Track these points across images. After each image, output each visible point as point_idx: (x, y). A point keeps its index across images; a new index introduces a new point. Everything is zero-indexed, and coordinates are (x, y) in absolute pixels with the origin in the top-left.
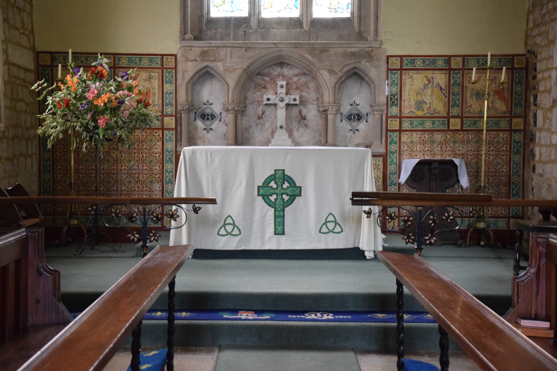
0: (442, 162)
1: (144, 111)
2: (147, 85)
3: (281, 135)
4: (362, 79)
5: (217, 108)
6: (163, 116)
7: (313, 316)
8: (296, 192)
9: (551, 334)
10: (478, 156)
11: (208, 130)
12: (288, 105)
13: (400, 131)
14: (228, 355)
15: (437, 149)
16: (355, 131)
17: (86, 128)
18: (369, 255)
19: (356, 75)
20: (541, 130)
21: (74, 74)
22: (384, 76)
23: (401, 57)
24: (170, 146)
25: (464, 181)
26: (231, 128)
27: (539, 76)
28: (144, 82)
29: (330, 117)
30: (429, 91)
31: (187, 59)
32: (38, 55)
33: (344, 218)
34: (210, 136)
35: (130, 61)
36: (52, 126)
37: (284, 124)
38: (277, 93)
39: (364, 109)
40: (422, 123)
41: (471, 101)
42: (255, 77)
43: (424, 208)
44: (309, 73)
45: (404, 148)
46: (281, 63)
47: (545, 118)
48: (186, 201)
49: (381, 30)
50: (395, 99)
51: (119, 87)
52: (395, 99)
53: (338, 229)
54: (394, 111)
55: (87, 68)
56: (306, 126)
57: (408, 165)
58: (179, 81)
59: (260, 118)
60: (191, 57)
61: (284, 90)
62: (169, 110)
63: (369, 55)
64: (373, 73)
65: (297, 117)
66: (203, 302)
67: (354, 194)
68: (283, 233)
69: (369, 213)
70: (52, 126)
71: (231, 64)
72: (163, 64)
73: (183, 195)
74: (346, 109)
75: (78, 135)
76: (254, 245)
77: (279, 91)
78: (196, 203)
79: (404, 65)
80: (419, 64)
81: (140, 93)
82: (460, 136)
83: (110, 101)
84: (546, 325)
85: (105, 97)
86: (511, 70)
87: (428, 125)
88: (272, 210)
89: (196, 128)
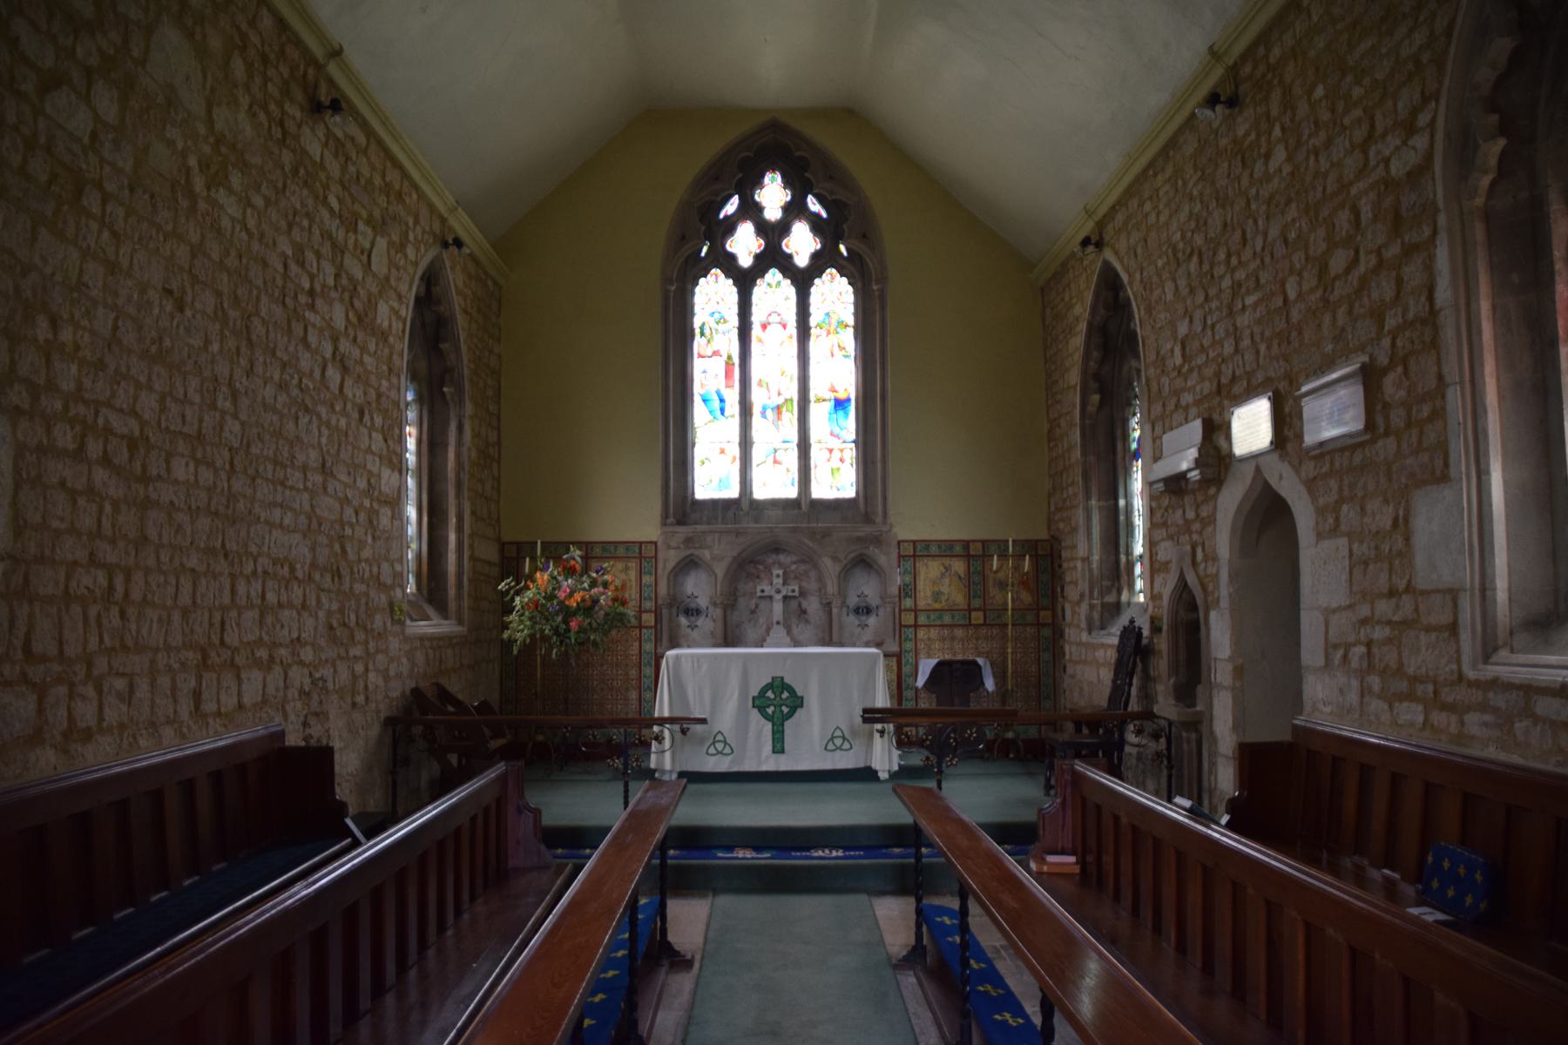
0: (963, 663)
1: (621, 609)
2: (623, 577)
3: (779, 632)
4: (870, 566)
5: (703, 602)
6: (641, 612)
7: (820, 853)
8: (797, 703)
9: (1077, 869)
10: (1004, 654)
11: (693, 627)
12: (785, 598)
13: (916, 626)
14: (725, 901)
15: (958, 646)
16: (864, 626)
17: (556, 631)
18: (883, 775)
19: (863, 562)
20: (1070, 625)
21: (544, 569)
22: (895, 563)
23: (914, 542)
24: (649, 647)
25: (990, 684)
26: (720, 624)
27: (1065, 565)
28: (618, 574)
29: (835, 611)
30: (947, 581)
31: (669, 547)
32: (503, 546)
33: (854, 733)
34: (695, 634)
35: (604, 550)
36: (519, 629)
37: (781, 619)
38: (773, 585)
39: (874, 601)
40: (940, 618)
41: (994, 591)
42: (747, 566)
43: (943, 721)
44: (809, 560)
45: (921, 646)
46: (777, 549)
47: (1074, 613)
48: (671, 720)
49: (891, 512)
50: (908, 590)
51: (593, 584)
52: (908, 590)
53: (846, 745)
54: (908, 603)
55: (558, 559)
56: (807, 621)
57: (926, 666)
58: (660, 571)
59: (753, 612)
60: (673, 544)
61: (780, 581)
62: (648, 605)
63: (877, 540)
64: (882, 560)
65: (796, 613)
66: (693, 838)
67: (865, 711)
68: (782, 752)
69: (882, 732)
70: (519, 629)
71: (719, 552)
72: (641, 553)
73: (666, 714)
74: (853, 601)
75: (545, 639)
76: (749, 766)
77: (775, 581)
78: (683, 724)
79: (918, 551)
80: (934, 549)
81: (617, 589)
82: (984, 631)
83: (583, 600)
84: (1072, 859)
85: (578, 597)
86: (1035, 558)
87: (947, 619)
88: (770, 725)
89: (679, 626)
